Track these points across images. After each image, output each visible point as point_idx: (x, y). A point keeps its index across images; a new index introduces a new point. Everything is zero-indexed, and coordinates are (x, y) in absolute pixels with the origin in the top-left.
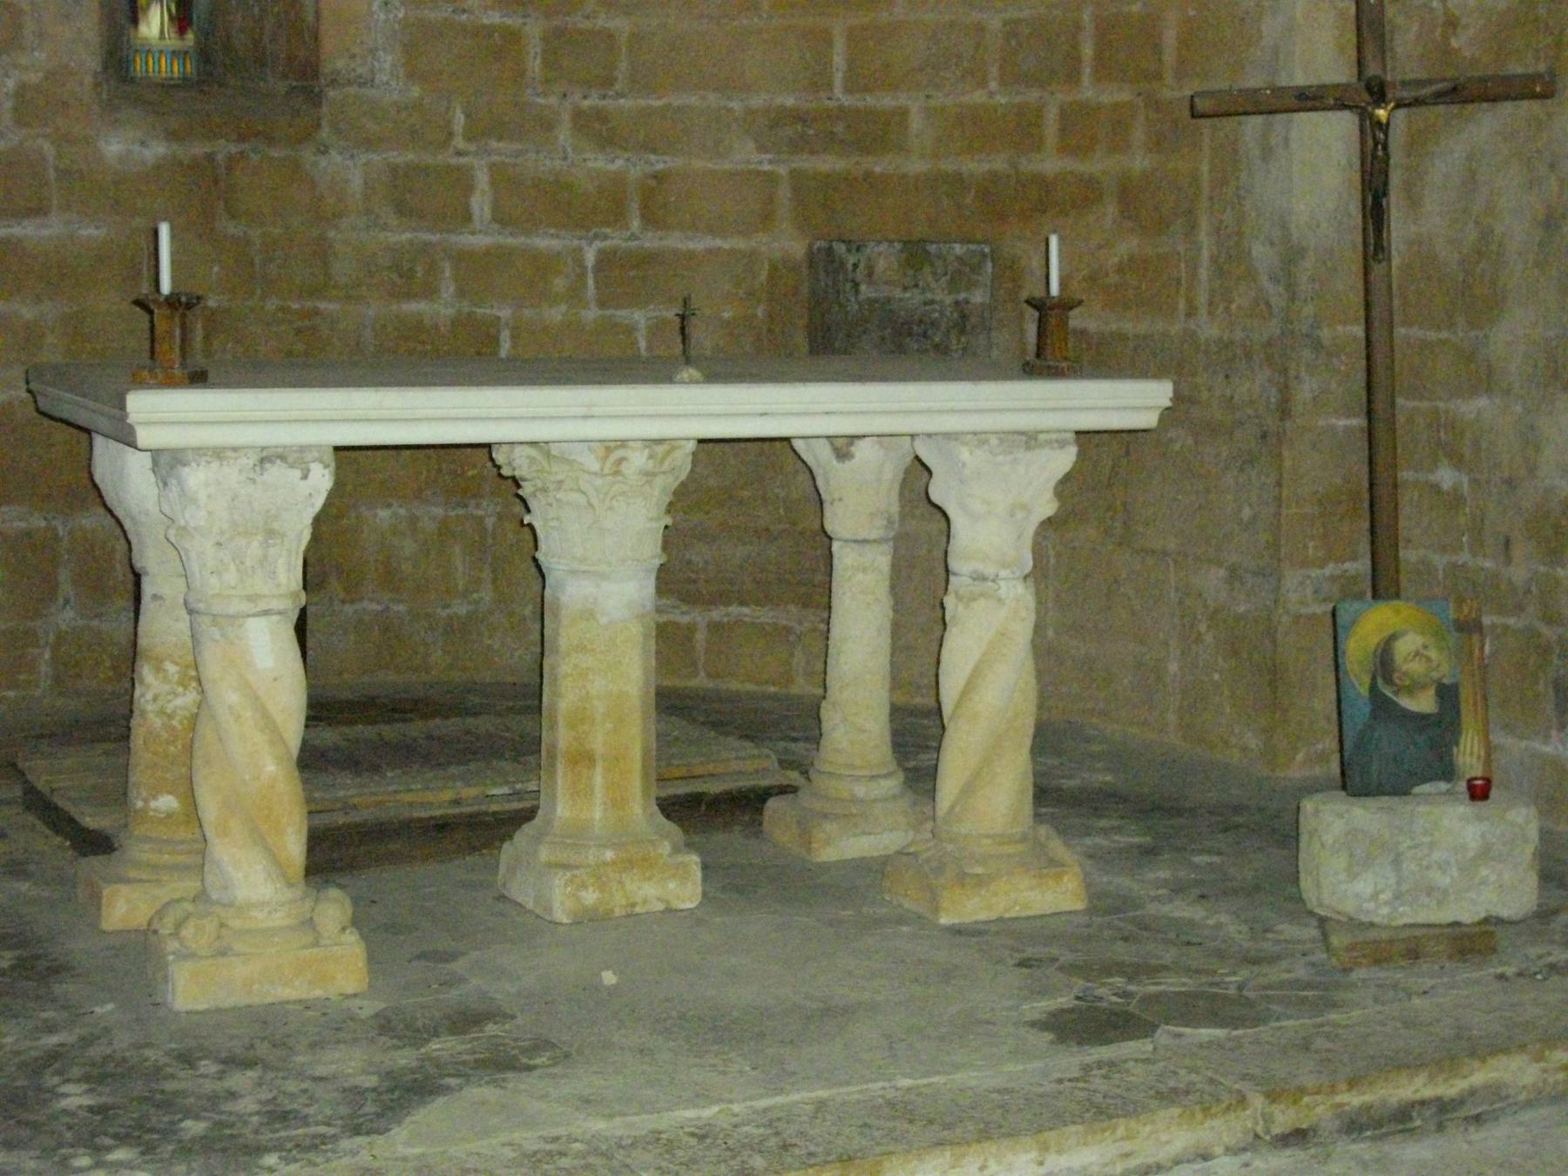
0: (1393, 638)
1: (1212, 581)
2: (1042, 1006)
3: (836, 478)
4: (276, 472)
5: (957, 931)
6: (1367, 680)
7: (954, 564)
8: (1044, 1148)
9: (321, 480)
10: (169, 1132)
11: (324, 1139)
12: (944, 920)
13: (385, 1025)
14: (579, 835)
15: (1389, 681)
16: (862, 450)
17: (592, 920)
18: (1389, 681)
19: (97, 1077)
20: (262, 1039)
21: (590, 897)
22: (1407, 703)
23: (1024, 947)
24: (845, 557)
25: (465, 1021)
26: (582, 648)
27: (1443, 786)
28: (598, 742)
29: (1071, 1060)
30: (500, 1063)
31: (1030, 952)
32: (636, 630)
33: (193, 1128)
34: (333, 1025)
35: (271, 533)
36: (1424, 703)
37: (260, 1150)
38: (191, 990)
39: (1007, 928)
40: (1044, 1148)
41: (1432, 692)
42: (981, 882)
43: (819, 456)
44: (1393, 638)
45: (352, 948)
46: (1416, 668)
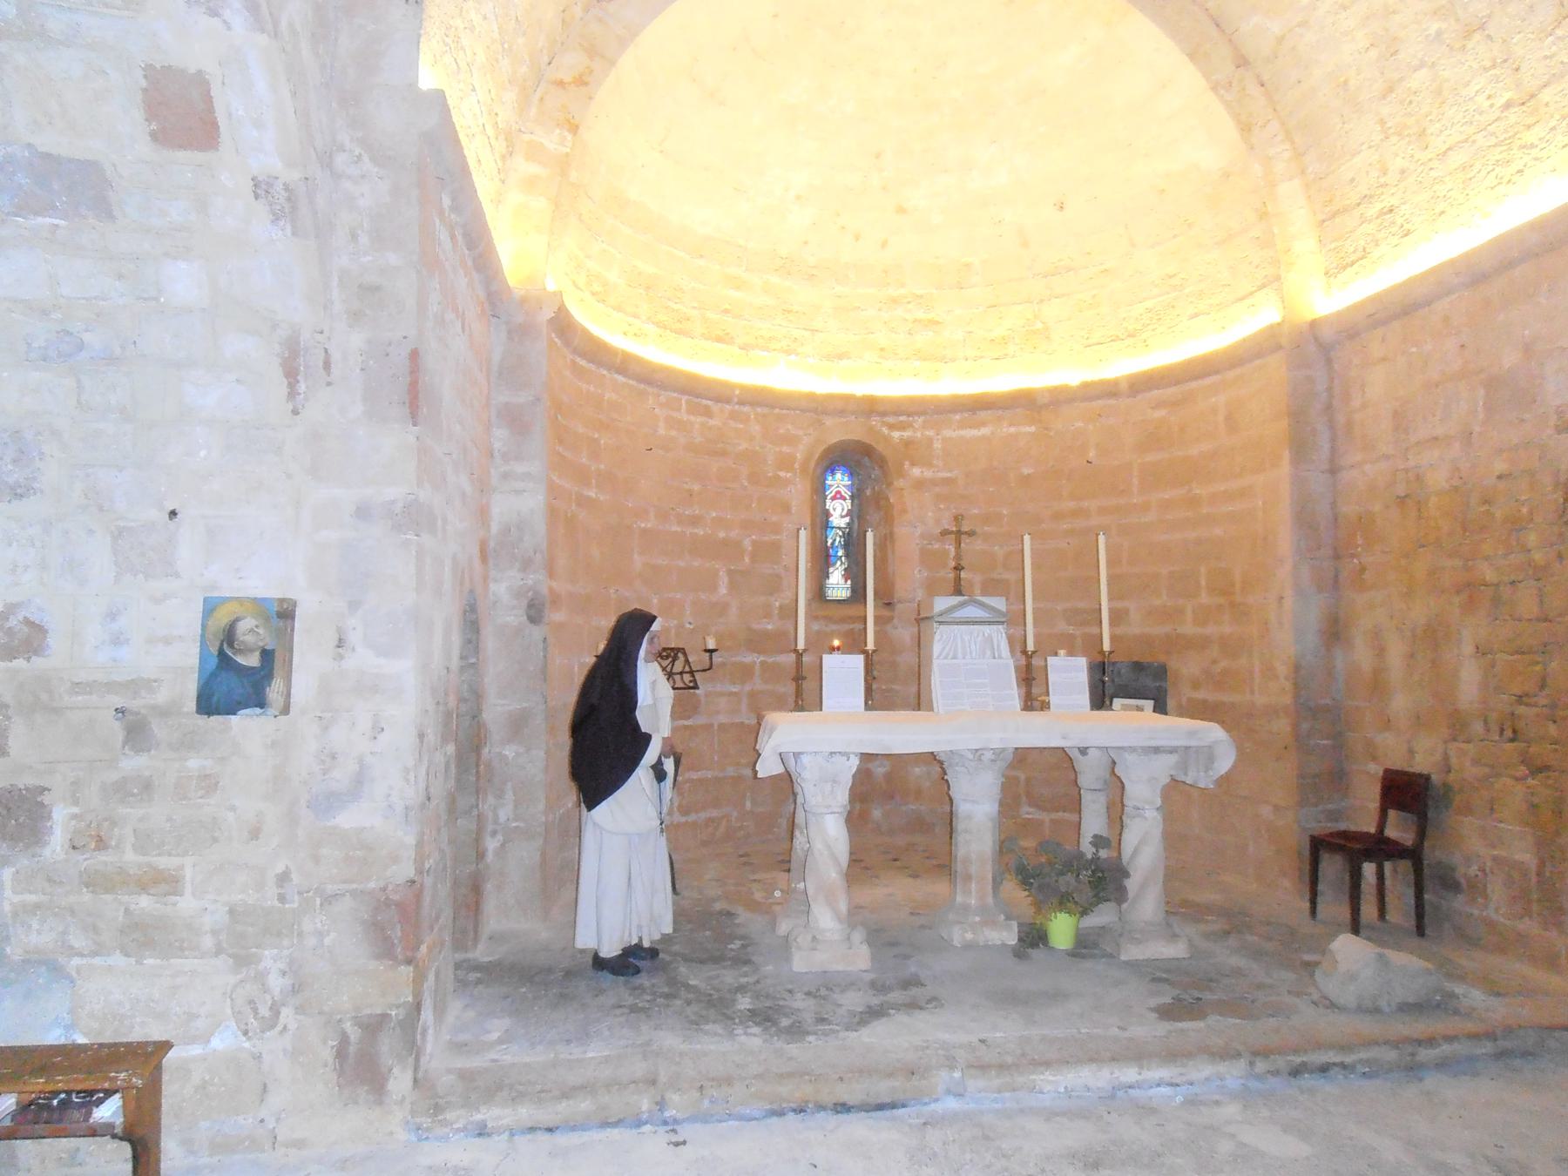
0: (237, 620)
1: (1266, 811)
2: (1153, 1002)
3: (1082, 763)
4: (837, 758)
5: (1127, 963)
6: (218, 644)
7: (1126, 802)
8: (1141, 1067)
9: (854, 762)
10: (775, 1023)
11: (833, 1031)
12: (1123, 958)
13: (873, 985)
14: (966, 908)
15: (231, 645)
16: (1090, 751)
17: (968, 946)
18: (231, 645)
19: (757, 996)
20: (824, 987)
21: (969, 936)
22: (240, 660)
23: (1158, 974)
24: (1087, 797)
25: (909, 983)
26: (966, 831)
27: (258, 710)
28: (973, 869)
29: (1163, 1028)
30: (913, 1006)
31: (1158, 974)
32: (990, 824)
33: (785, 1022)
34: (849, 983)
35: (834, 781)
36: (253, 661)
37: (808, 1033)
38: (801, 962)
39: (1149, 962)
40: (1141, 1067)
41: (257, 654)
42: (1139, 942)
43: (1075, 754)
44: (237, 620)
45: (864, 950)
46: (249, 639)
